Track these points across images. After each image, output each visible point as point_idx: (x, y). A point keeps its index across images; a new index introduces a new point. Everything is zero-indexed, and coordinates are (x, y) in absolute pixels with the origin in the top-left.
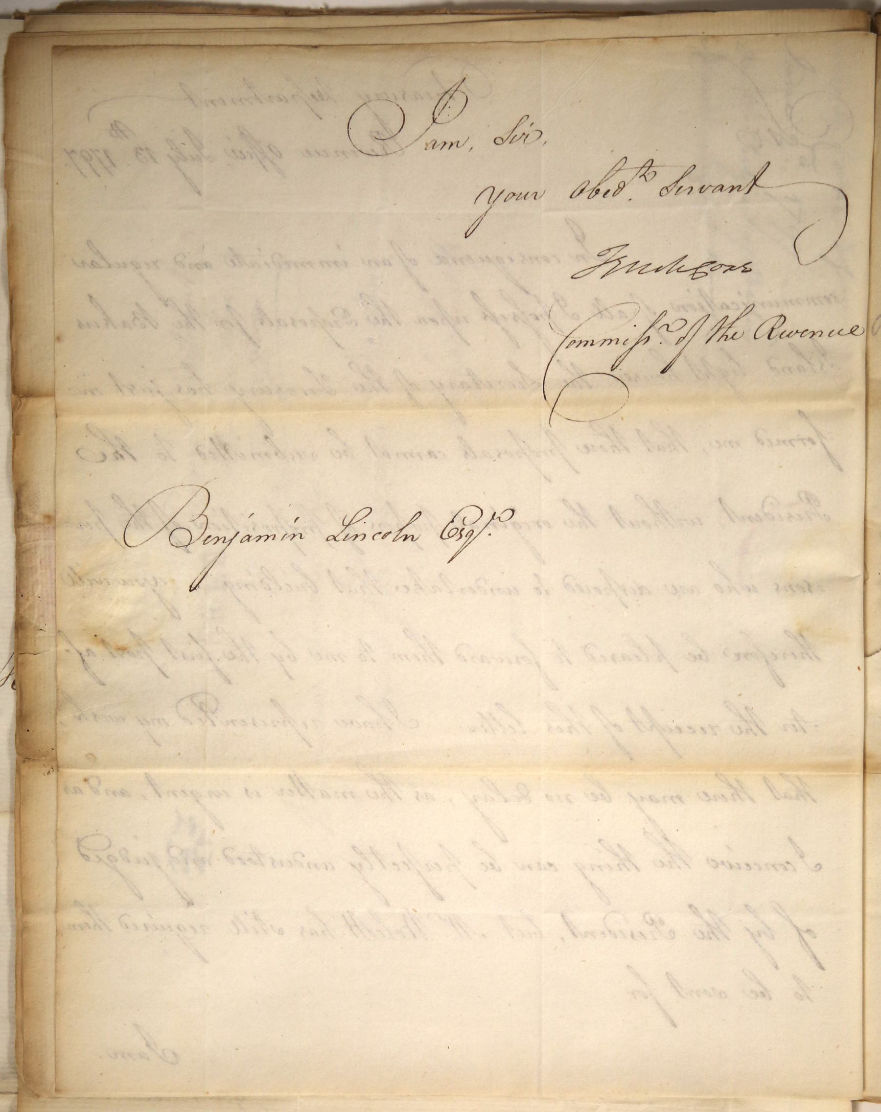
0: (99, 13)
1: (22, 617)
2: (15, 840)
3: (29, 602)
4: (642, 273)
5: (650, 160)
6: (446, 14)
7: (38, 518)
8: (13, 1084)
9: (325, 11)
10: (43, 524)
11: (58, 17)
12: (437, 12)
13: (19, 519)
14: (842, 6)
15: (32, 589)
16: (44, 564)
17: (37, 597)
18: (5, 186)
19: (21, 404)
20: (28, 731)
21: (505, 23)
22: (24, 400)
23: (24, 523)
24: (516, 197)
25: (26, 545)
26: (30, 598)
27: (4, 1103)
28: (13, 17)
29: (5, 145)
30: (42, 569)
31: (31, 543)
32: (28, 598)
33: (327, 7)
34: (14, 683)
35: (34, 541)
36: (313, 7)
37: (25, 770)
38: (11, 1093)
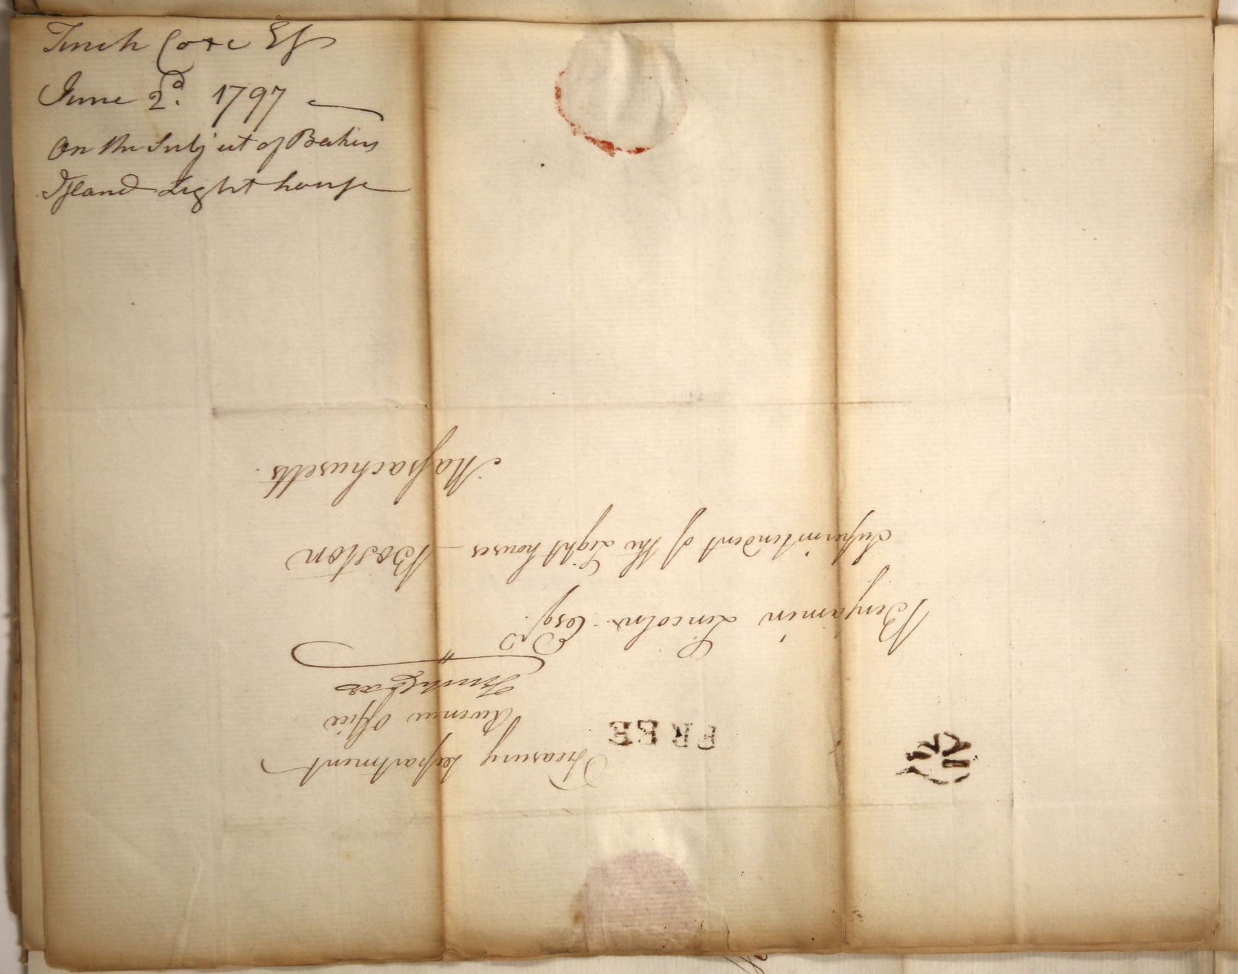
0: (20, 868)
1: (688, 947)
2: (937, 953)
3: (670, 938)
4: (279, 139)
6: (18, 484)
7: (578, 930)
8: (1203, 956)
9: (15, 619)
10: (585, 923)
11: (25, 912)
12: (16, 494)
13: (579, 951)
14: (7, 45)
15: (656, 935)
16: (628, 923)
17: (665, 930)
19: (452, 949)
21: (29, 415)
22: (448, 946)
23: (583, 945)
28: (26, 964)
30: (634, 925)
34: (759, 958)
35: (603, 933)
38: (1214, 958)
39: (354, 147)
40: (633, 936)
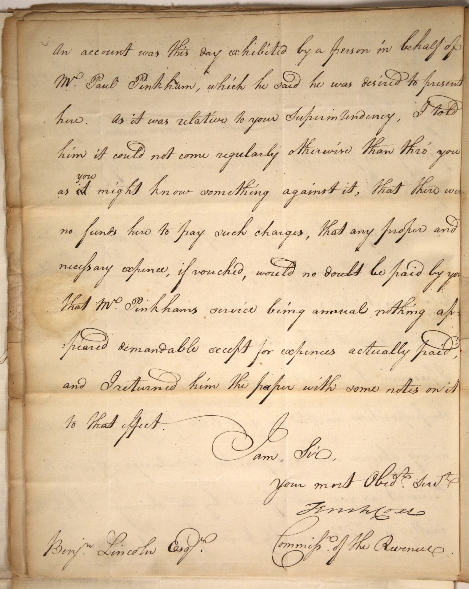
3: (14, 316)
5: (369, 52)
9: (172, 7)
15: (16, 308)
17: (18, 313)
18: (2, 96)
19: (10, 211)
20: (14, 383)
22: (12, 209)
24: (179, 193)
25: (13, 285)
26: (15, 313)
27: (4, 584)
29: (2, 75)
31: (15, 284)
32: (13, 313)
33: (173, 5)
35: (17, 283)
36: (165, 5)
37: (466, 10)
38: (9, 579)
39: (443, 229)
40: (16, 297)
